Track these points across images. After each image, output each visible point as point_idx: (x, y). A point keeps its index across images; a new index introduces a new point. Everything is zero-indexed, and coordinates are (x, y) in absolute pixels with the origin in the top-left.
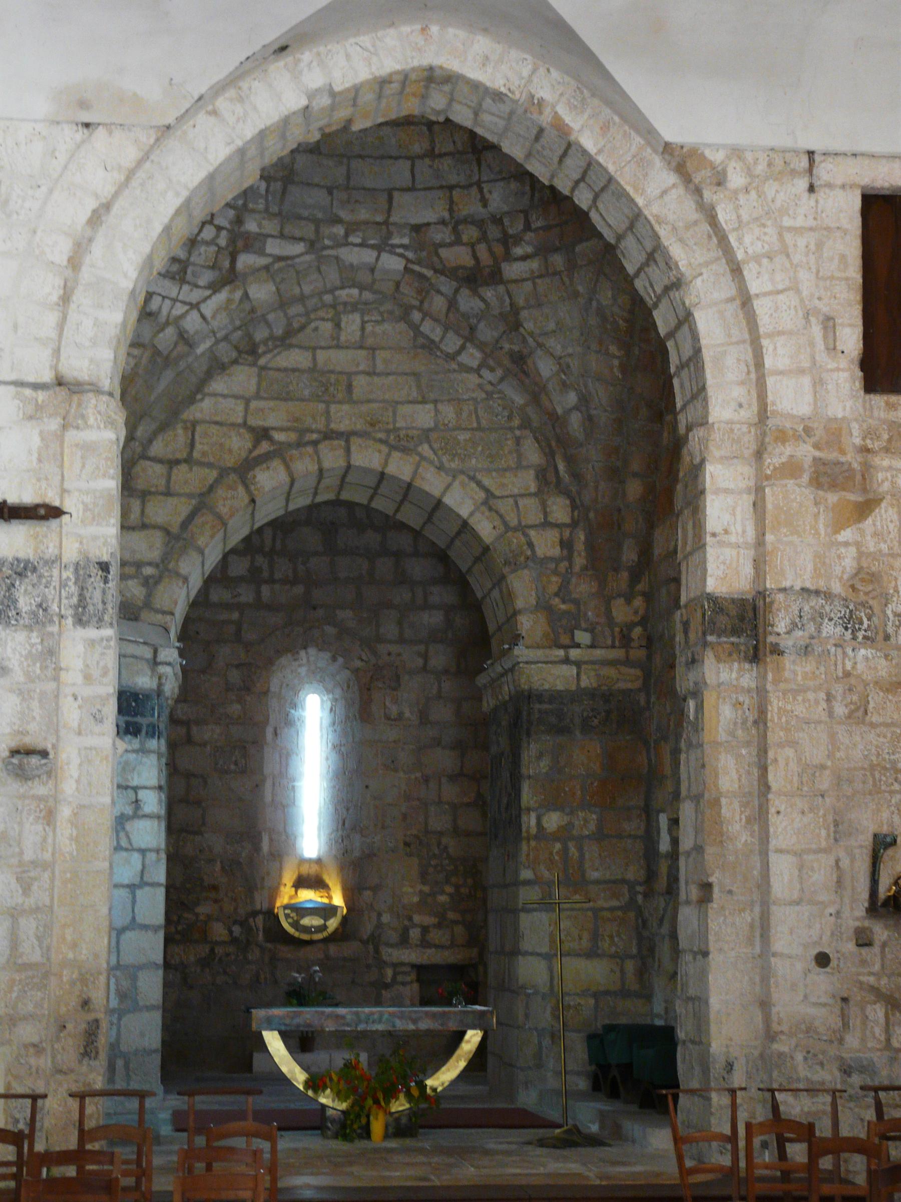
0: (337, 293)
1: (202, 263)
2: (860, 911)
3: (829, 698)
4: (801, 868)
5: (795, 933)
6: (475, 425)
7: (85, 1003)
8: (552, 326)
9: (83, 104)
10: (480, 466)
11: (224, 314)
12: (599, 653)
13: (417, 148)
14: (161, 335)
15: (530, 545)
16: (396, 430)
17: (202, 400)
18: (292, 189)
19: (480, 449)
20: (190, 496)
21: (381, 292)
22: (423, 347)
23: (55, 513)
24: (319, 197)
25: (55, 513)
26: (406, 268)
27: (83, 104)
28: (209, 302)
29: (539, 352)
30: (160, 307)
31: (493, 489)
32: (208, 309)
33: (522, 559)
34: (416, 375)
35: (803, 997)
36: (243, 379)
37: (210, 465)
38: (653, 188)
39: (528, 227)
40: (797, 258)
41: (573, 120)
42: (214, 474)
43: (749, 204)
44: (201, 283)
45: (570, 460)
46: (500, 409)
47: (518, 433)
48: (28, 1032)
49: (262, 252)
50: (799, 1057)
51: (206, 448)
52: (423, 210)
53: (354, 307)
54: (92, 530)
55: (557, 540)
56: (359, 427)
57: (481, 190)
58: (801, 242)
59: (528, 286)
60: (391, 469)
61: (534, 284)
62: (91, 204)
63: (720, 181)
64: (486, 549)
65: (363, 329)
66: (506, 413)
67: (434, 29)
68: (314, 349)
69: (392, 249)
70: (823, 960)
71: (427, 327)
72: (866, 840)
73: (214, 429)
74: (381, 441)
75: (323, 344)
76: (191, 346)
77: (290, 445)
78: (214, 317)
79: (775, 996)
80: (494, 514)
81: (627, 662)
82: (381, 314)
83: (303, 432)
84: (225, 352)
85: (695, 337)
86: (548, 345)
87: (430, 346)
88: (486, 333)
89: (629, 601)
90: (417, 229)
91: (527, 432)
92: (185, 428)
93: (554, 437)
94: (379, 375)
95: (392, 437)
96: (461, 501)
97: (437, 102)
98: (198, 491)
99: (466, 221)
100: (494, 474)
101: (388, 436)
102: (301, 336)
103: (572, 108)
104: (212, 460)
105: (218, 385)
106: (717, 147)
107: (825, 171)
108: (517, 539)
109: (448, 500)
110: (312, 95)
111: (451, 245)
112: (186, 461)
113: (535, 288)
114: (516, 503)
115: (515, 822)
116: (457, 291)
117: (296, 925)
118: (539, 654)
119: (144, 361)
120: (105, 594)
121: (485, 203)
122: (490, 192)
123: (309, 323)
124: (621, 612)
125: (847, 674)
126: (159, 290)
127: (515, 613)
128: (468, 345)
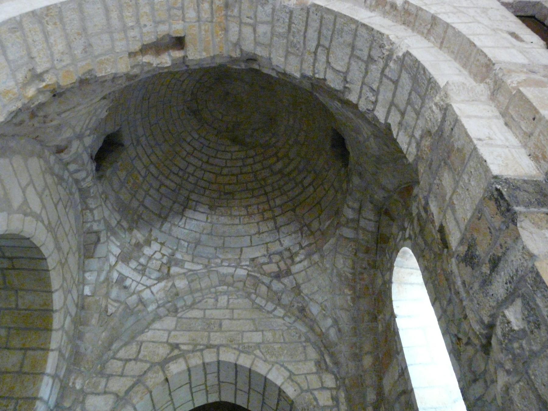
0: (217, 288)
1: (153, 267)
6: (282, 341)
8: (316, 288)
10: (286, 360)
11: (162, 292)
13: (253, 232)
14: (130, 298)
15: (316, 399)
16: (243, 343)
17: (148, 332)
18: (198, 246)
19: (285, 352)
20: (133, 376)
21: (237, 287)
22: (257, 308)
24: (212, 250)
26: (248, 274)
28: (155, 286)
29: (311, 303)
30: (131, 285)
31: (293, 371)
32: (155, 289)
33: (312, 407)
34: (253, 320)
36: (169, 322)
37: (146, 361)
42: (148, 365)
44: (153, 277)
45: (332, 355)
46: (295, 333)
47: (304, 344)
49: (182, 267)
51: (146, 353)
55: (330, 396)
56: (224, 342)
57: (280, 241)
60: (240, 362)
61: (306, 272)
65: (228, 301)
66: (298, 335)
68: (205, 309)
69: (242, 267)
71: (258, 300)
73: (151, 345)
74: (235, 349)
75: (209, 307)
76: (145, 306)
77: (188, 351)
78: (157, 293)
80: (295, 383)
82: (237, 296)
83: (195, 345)
84: (162, 311)
86: (315, 299)
87: (260, 308)
88: (286, 299)
90: (253, 260)
91: (308, 344)
92: (137, 344)
93: (325, 346)
94: (235, 320)
95: (241, 347)
96: (277, 377)
98: (138, 374)
99: (274, 254)
100: (293, 363)
101: (239, 347)
102: (199, 304)
104: (148, 359)
105: (157, 325)
108: (308, 396)
109: (270, 377)
111: (268, 263)
112: (134, 360)
113: (307, 274)
114: (306, 377)
116: (271, 282)
119: (120, 310)
121: (281, 245)
122: (284, 241)
123: (203, 299)
126: (130, 276)
128: (278, 307)
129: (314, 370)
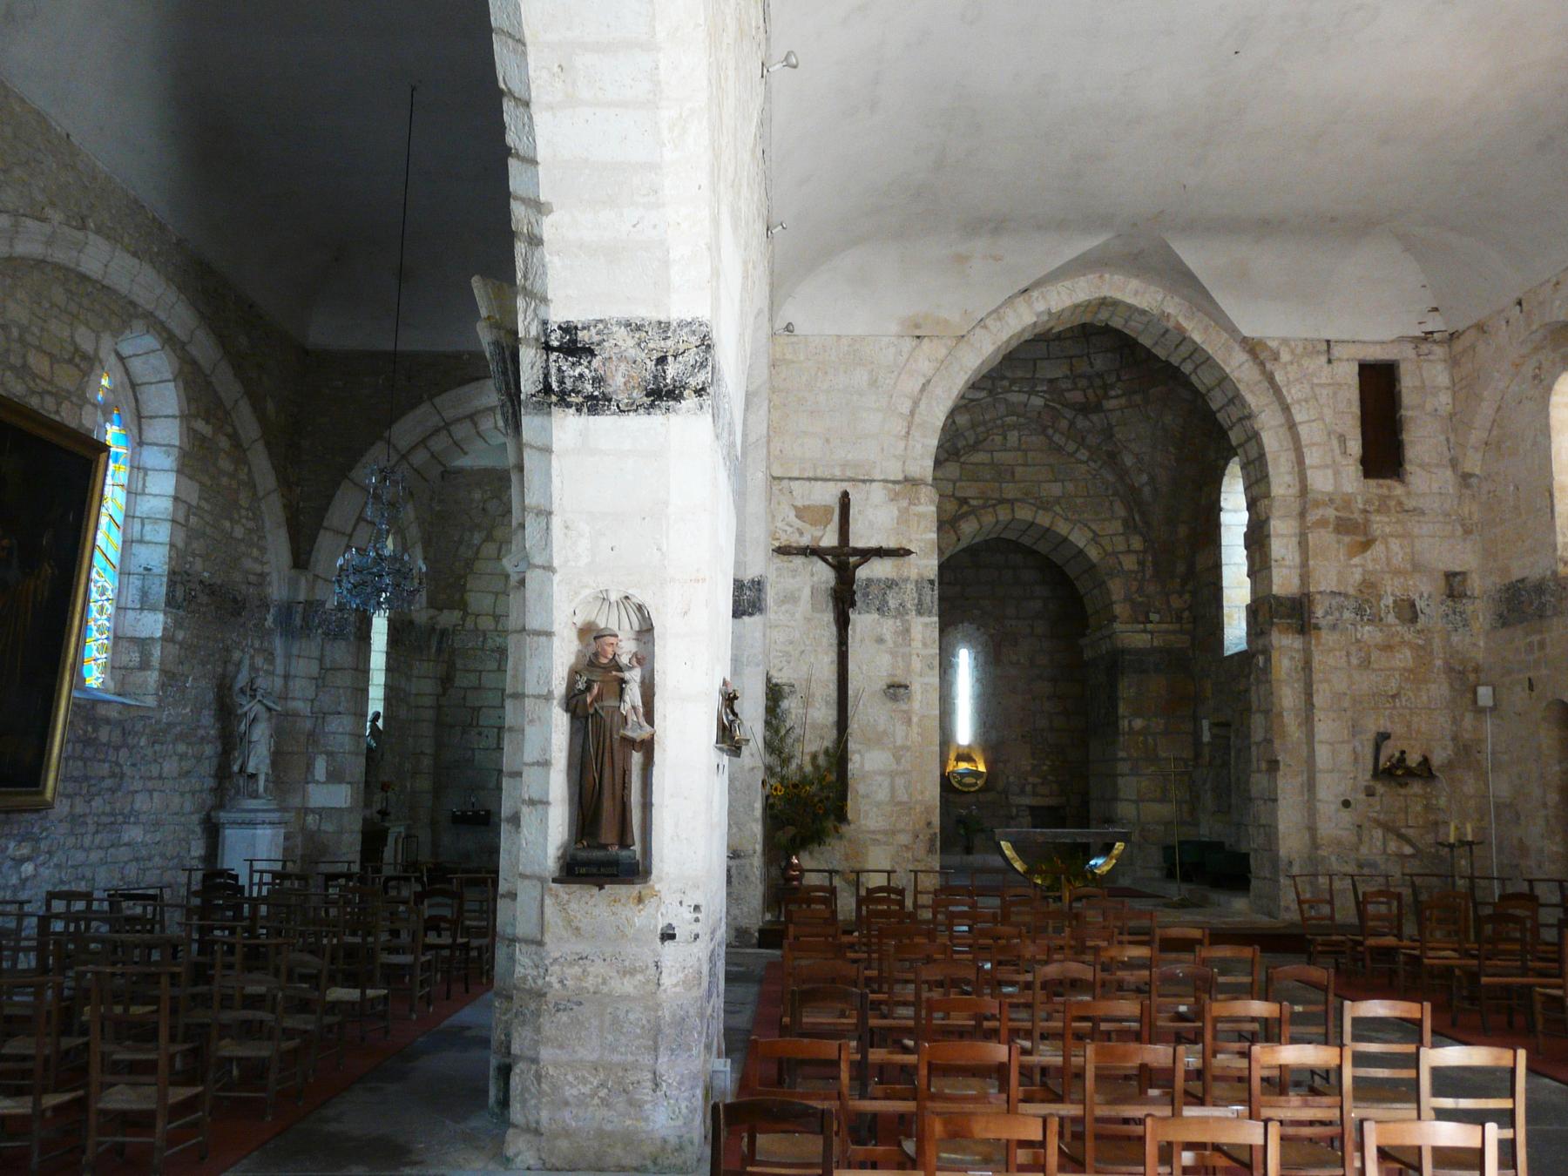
2: (1368, 775)
3: (1348, 654)
4: (1333, 752)
5: (1329, 790)
7: (929, 824)
9: (917, 326)
12: (1164, 626)
23: (908, 552)
25: (908, 552)
26: (1046, 405)
27: (917, 326)
35: (1334, 824)
38: (1235, 363)
39: (1119, 379)
40: (1322, 401)
41: (1188, 325)
43: (1292, 369)
48: (904, 839)
50: (1333, 858)
52: (1057, 371)
53: (1015, 427)
54: (925, 562)
58: (1325, 392)
59: (1119, 413)
60: (1039, 520)
62: (923, 380)
63: (1276, 357)
64: (1094, 566)
67: (1107, 276)
69: (1037, 394)
70: (1346, 804)
71: (1056, 438)
72: (1370, 736)
79: (1319, 824)
81: (1181, 631)
85: (1261, 446)
87: (1060, 449)
88: (1092, 440)
89: (1181, 595)
90: (1051, 381)
93: (1132, 498)
96: (1079, 538)
97: (1103, 316)
99: (1080, 376)
103: (1186, 317)
106: (1273, 339)
107: (1337, 351)
110: (1038, 315)
115: (1116, 724)
117: (959, 782)
118: (1129, 627)
120: (932, 597)
124: (1176, 602)
125: (1358, 641)
127: (1112, 603)
129: (1121, 530)
